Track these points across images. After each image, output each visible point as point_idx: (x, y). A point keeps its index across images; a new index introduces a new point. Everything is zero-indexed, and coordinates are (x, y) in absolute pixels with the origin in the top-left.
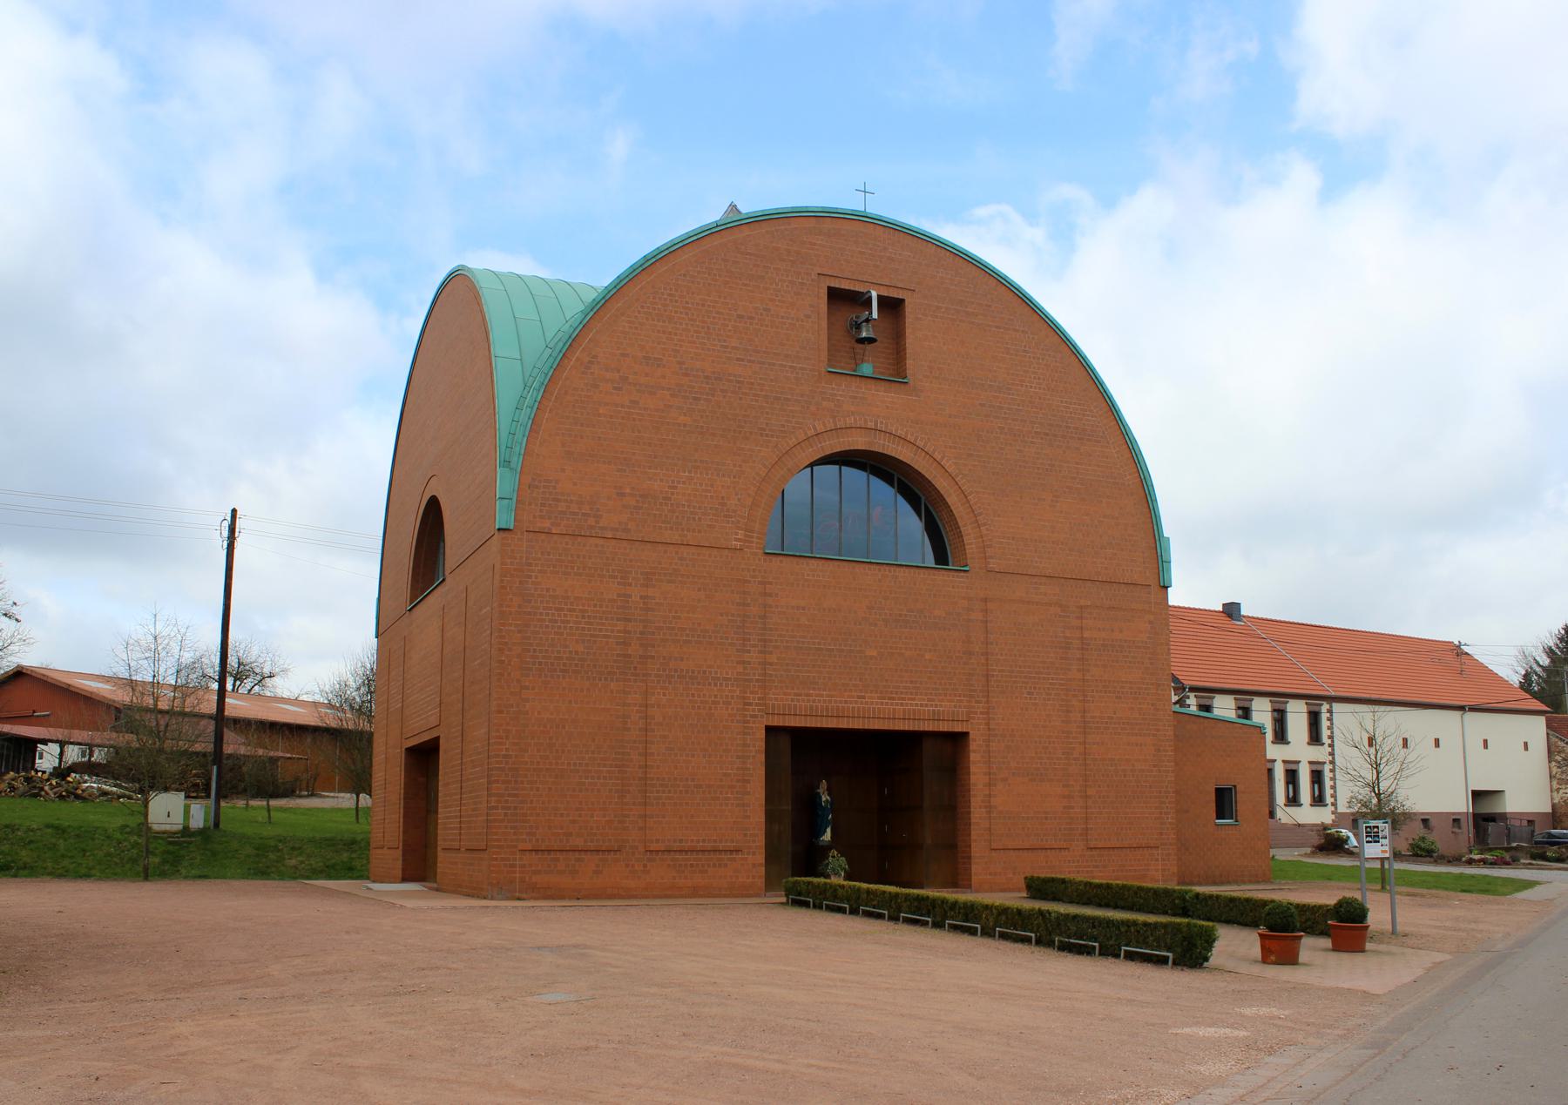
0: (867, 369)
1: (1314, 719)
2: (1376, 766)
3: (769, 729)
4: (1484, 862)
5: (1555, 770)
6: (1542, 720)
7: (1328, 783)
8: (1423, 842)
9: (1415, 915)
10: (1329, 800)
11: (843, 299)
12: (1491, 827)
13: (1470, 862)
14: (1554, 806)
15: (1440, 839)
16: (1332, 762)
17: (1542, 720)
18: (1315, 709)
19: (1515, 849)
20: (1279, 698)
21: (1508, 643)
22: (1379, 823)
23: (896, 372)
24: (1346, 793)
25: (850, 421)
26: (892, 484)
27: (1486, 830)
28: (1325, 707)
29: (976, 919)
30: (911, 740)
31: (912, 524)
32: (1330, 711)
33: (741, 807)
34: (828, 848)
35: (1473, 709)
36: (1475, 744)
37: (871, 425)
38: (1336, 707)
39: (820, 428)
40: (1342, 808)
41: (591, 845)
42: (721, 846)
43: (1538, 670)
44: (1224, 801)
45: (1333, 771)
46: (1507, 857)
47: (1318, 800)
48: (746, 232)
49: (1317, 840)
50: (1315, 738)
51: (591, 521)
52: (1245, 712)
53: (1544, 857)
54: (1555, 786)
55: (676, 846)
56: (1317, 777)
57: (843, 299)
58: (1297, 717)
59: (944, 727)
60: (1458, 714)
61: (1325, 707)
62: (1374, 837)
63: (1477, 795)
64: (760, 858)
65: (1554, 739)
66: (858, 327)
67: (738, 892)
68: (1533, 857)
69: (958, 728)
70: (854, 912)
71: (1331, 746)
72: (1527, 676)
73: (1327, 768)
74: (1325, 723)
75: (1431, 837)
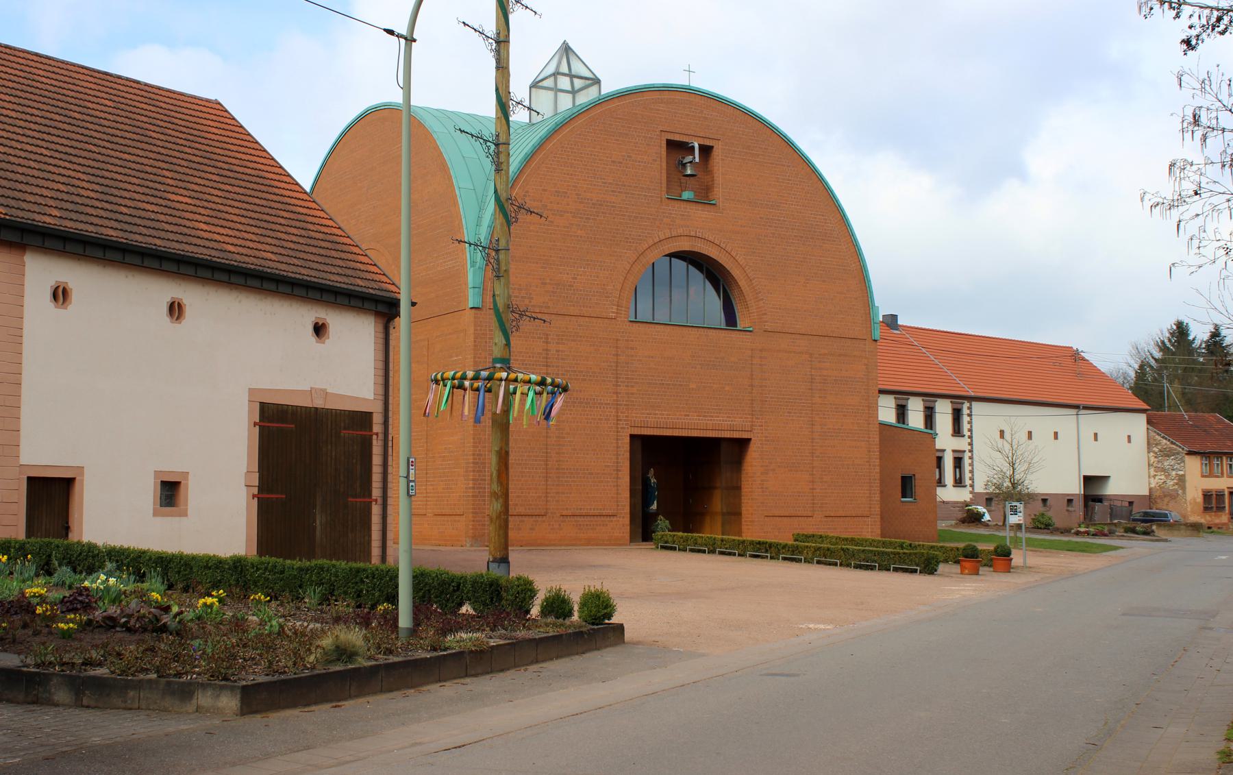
0: (687, 195)
1: (957, 415)
2: (1013, 465)
3: (632, 436)
4: (1087, 533)
5: (1152, 459)
6: (1142, 418)
7: (967, 468)
8: (1048, 520)
9: (1034, 559)
10: (968, 482)
11: (677, 147)
12: (1098, 506)
13: (1078, 533)
14: (1150, 489)
15: (1057, 516)
16: (971, 451)
17: (1142, 418)
18: (958, 406)
19: (1115, 525)
20: (930, 399)
21: (1117, 349)
22: (1017, 504)
23: (705, 197)
24: (982, 477)
25: (680, 231)
26: (702, 271)
27: (1093, 508)
28: (966, 405)
29: (801, 553)
30: (716, 442)
31: (714, 303)
32: (970, 408)
33: (613, 486)
34: (656, 515)
35: (1086, 408)
36: (1087, 435)
37: (693, 234)
38: (976, 406)
39: (662, 237)
40: (979, 488)
41: (529, 512)
42: (604, 512)
43: (1153, 363)
44: (907, 485)
45: (971, 458)
46: (1106, 530)
47: (959, 482)
48: (617, 103)
49: (961, 515)
50: (957, 431)
51: (527, 302)
52: (902, 412)
53: (1133, 531)
54: (1152, 473)
55: (578, 512)
56: (958, 462)
57: (677, 147)
58: (944, 410)
59: (736, 435)
60: (1074, 411)
61: (966, 405)
62: (1015, 511)
63: (1088, 480)
64: (627, 520)
65: (1152, 434)
66: (684, 165)
67: (612, 543)
68: (1127, 530)
69: (745, 436)
70: (712, 552)
71: (970, 437)
72: (1141, 367)
73: (967, 455)
74: (965, 419)
75: (1050, 514)
